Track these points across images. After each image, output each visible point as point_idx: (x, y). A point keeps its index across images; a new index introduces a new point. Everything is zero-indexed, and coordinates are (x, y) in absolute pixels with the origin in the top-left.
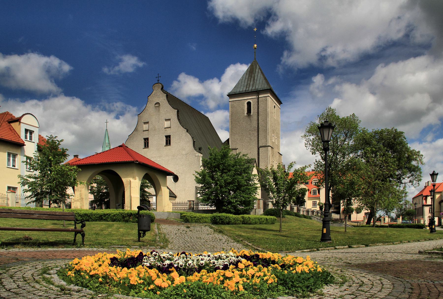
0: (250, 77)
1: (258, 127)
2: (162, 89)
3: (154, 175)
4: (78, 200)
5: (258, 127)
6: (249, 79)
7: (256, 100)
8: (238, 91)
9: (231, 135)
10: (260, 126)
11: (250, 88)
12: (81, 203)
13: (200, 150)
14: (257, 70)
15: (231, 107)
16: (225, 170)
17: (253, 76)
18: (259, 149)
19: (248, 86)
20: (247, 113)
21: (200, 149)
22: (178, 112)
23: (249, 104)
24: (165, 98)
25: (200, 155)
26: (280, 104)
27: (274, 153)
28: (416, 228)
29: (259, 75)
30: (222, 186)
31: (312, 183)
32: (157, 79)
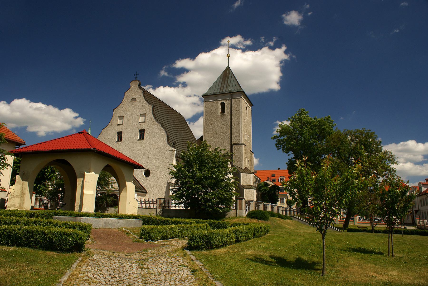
0: (224, 81)
1: (231, 125)
2: (139, 85)
3: (117, 167)
4: (17, 196)
5: (231, 125)
7: (230, 101)
8: (212, 92)
9: (205, 133)
10: (233, 125)
11: (224, 90)
12: (21, 200)
13: (173, 145)
16: (202, 164)
17: (226, 80)
19: (222, 89)
20: (221, 113)
21: (174, 144)
22: (153, 106)
23: (223, 105)
24: (142, 94)
25: (173, 149)
27: (247, 150)
30: (274, 201)
31: (279, 181)
32: (135, 76)
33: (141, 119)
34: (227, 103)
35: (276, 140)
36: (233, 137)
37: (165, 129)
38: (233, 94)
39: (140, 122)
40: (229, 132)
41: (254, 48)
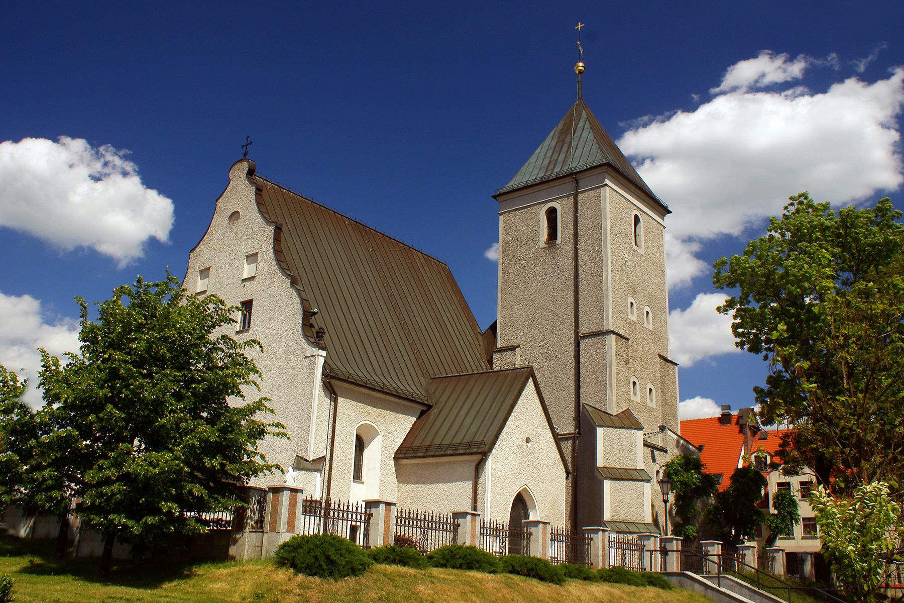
1: (576, 276)
5: (576, 276)
6: (557, 149)
10: (581, 273)
11: (557, 170)
14: (581, 124)
15: (505, 230)
17: (568, 139)
18: (577, 345)
21: (320, 334)
23: (552, 214)
25: (316, 351)
26: (662, 216)
28: (362, 454)
29: (585, 134)
32: (243, 151)
33: (247, 270)
34: (562, 207)
35: (732, 312)
36: (581, 315)
37: (298, 292)
38: (579, 176)
39: (244, 280)
40: (571, 300)
41: (817, 82)
